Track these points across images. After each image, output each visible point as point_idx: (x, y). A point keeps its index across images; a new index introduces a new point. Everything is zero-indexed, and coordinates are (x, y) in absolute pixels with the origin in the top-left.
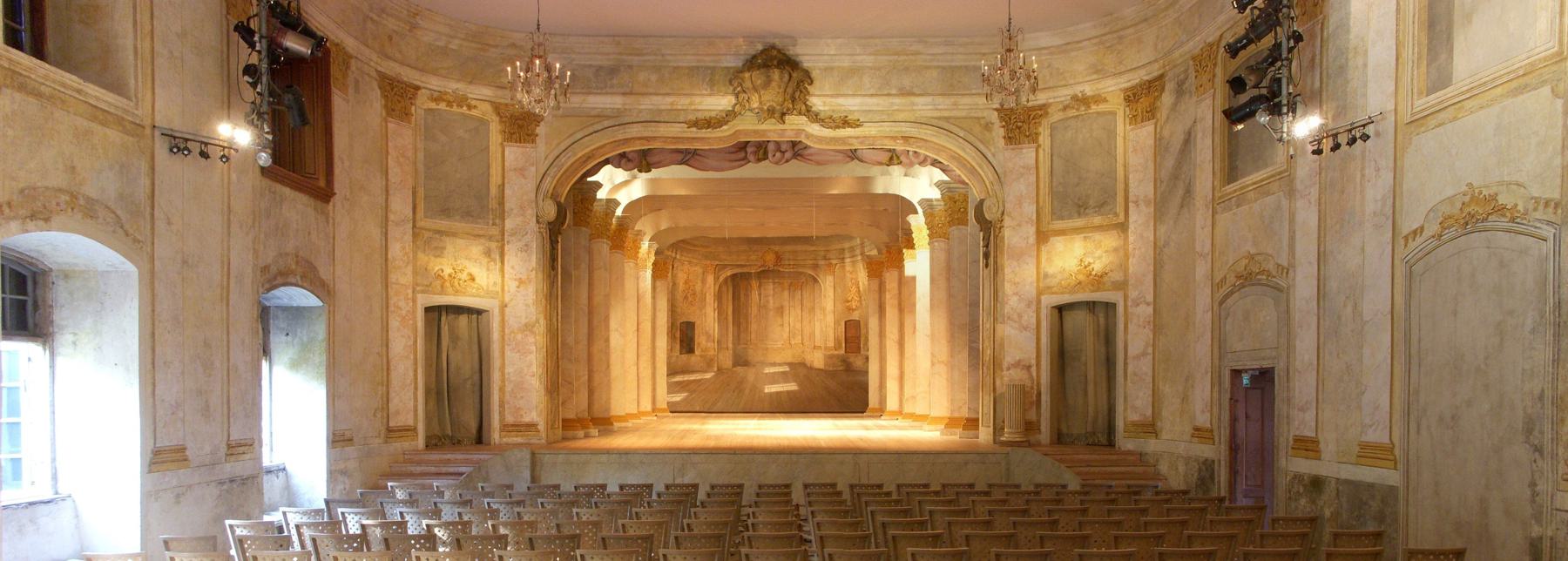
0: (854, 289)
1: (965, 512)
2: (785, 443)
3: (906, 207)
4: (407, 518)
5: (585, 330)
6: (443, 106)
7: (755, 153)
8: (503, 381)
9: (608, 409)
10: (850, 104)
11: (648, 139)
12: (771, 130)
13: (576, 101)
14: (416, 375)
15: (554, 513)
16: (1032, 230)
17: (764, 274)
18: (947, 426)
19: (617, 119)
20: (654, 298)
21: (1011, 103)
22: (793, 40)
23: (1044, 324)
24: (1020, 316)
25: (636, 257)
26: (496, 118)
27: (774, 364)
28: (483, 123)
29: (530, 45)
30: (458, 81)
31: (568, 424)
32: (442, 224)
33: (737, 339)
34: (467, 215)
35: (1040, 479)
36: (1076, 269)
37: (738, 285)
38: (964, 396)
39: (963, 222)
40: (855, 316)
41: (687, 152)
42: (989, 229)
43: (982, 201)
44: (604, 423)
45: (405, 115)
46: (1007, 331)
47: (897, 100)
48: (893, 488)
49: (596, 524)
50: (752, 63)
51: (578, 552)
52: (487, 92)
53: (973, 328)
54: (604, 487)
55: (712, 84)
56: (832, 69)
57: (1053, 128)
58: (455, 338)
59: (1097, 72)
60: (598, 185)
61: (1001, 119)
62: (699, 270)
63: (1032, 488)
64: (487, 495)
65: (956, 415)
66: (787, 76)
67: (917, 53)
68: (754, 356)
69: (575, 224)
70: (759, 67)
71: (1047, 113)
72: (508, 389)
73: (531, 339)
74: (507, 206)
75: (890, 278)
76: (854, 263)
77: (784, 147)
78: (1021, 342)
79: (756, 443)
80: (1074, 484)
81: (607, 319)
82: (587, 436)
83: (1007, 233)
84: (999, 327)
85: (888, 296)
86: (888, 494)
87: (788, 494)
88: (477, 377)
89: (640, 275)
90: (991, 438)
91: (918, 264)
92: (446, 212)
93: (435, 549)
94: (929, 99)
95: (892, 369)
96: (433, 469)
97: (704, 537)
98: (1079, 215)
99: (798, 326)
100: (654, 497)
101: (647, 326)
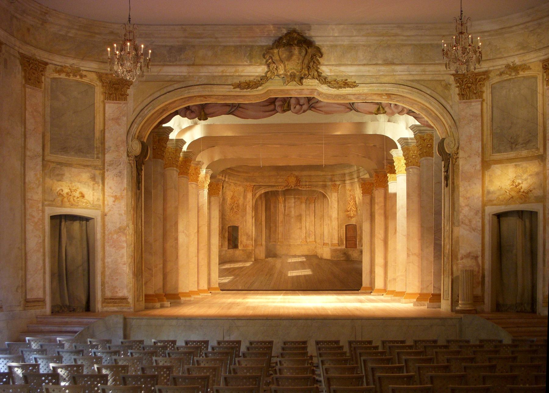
0: (352, 203)
1: (430, 360)
2: (303, 312)
3: (389, 143)
4: (40, 362)
5: (160, 232)
6: (63, 76)
7: (281, 106)
8: (104, 267)
9: (177, 288)
10: (349, 71)
11: (205, 97)
12: (293, 90)
13: (155, 70)
14: (44, 260)
15: (140, 360)
16: (478, 160)
17: (287, 192)
18: (418, 299)
19: (184, 84)
20: (209, 209)
21: (463, 70)
22: (309, 26)
23: (487, 227)
24: (470, 221)
25: (197, 180)
26: (99, 84)
27: (295, 256)
28: (91, 87)
29: (124, 32)
30: (75, 58)
31: (149, 298)
32: (63, 158)
33: (269, 238)
34: (79, 151)
35: (484, 336)
36: (509, 187)
37: (269, 200)
38: (431, 278)
39: (430, 154)
40: (353, 221)
41: (233, 105)
42: (449, 159)
43: (443, 140)
44: (175, 298)
45: (37, 83)
46: (461, 232)
47: (383, 68)
48: (379, 344)
49: (169, 368)
50: (279, 43)
51: (157, 387)
52: (94, 66)
53: (437, 231)
54: (174, 342)
55: (251, 57)
56: (336, 46)
57: (493, 88)
58: (70, 237)
59: (524, 48)
60: (170, 130)
61: (457, 81)
62: (241, 189)
63: (478, 343)
64: (93, 347)
65: (425, 292)
66: (304, 52)
67: (396, 35)
68: (281, 250)
69: (154, 157)
70: (284, 45)
71: (488, 78)
72: (108, 272)
73: (124, 239)
74: (107, 145)
75: (378, 194)
76: (352, 184)
77: (302, 102)
78: (470, 239)
79: (282, 312)
80: (507, 339)
81: (176, 223)
82: (162, 307)
83: (461, 162)
84: (456, 229)
85: (377, 207)
86: (376, 348)
87: (305, 348)
88: (86, 265)
89: (199, 193)
90: (449, 308)
91: (399, 184)
92: (64, 150)
93: (58, 383)
94: (405, 67)
95: (379, 260)
96: (56, 328)
97: (245, 378)
98: (512, 149)
99: (312, 228)
100: (210, 350)
101: (204, 229)
